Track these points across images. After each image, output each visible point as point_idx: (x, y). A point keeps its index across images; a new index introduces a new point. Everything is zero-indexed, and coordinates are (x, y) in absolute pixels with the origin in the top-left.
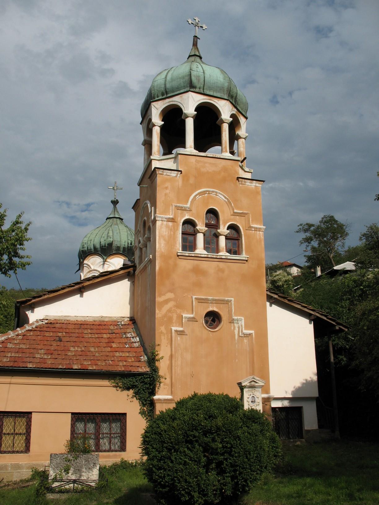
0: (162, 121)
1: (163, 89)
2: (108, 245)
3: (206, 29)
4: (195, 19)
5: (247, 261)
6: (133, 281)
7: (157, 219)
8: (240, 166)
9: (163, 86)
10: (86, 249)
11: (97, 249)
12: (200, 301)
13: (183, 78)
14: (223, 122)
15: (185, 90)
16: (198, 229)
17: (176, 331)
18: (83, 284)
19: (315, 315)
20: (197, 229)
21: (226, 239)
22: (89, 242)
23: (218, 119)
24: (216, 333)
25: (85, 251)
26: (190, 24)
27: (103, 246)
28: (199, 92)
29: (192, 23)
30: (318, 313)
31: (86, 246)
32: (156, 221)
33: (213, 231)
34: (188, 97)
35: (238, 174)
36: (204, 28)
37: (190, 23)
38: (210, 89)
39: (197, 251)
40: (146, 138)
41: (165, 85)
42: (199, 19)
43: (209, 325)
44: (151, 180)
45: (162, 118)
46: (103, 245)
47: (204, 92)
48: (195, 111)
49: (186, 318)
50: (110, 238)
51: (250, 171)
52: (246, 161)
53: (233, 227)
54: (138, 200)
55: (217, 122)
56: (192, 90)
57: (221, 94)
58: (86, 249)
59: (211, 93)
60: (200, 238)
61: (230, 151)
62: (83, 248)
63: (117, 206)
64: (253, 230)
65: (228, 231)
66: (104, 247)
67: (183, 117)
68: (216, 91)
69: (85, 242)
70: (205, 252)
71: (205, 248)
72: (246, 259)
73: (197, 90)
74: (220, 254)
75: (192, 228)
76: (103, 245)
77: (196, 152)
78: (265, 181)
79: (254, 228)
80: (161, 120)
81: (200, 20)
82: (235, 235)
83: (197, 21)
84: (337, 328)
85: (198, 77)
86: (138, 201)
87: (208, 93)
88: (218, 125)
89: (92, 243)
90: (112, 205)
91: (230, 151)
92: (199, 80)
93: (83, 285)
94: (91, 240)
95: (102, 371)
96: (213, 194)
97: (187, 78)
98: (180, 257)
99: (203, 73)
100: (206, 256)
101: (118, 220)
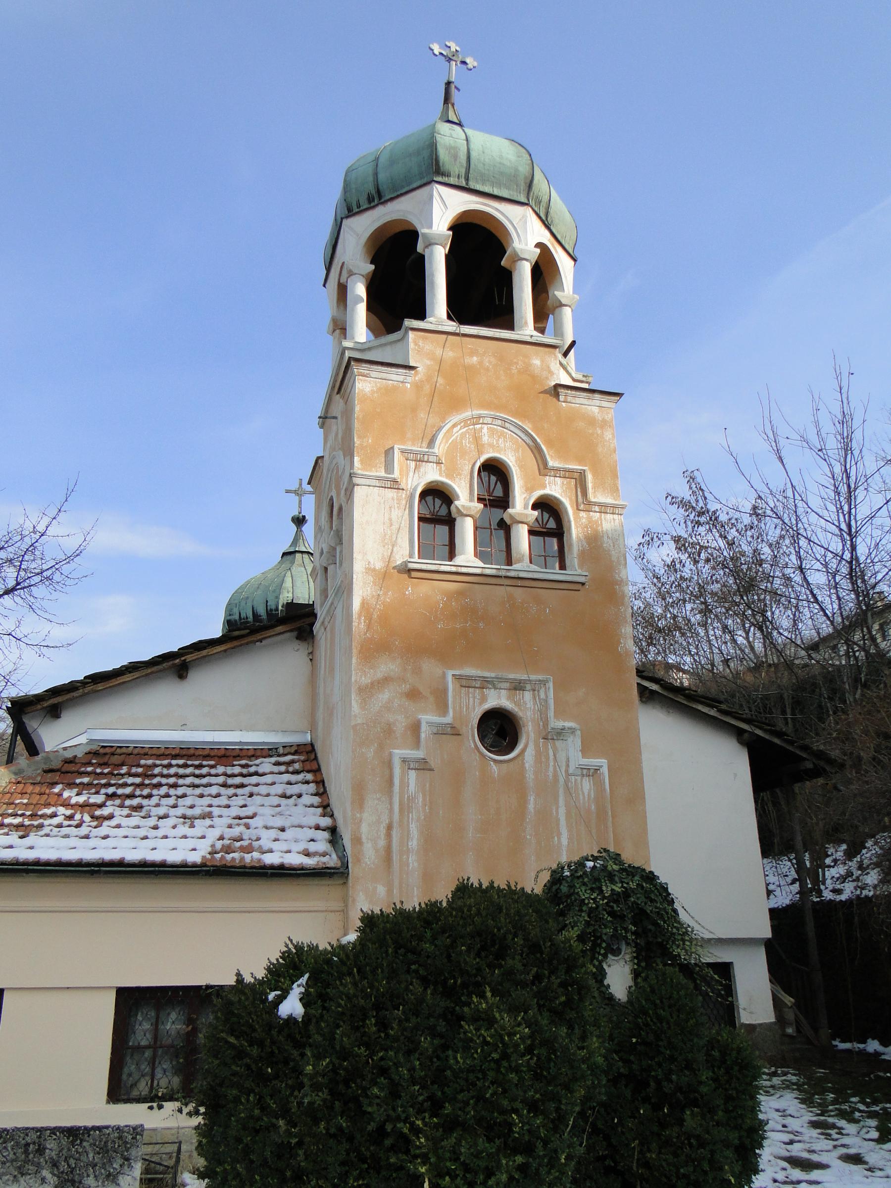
0: (371, 263)
1: (371, 189)
2: (282, 607)
3: (474, 67)
4: (448, 44)
5: (583, 584)
6: (310, 651)
7: (356, 480)
8: (561, 364)
9: (371, 179)
10: (237, 617)
11: (260, 616)
12: (465, 682)
13: (418, 153)
14: (517, 258)
15: (425, 180)
16: (460, 507)
17: (404, 761)
18: (183, 658)
19: (752, 734)
20: (457, 507)
21: (531, 532)
22: (243, 603)
23: (504, 252)
24: (511, 764)
25: (236, 621)
26: (436, 56)
27: (271, 610)
28: (457, 184)
29: (441, 54)
30: (761, 728)
31: (236, 611)
32: (354, 485)
33: (497, 514)
34: (431, 198)
35: (558, 379)
36: (470, 66)
37: (436, 52)
38: (484, 180)
39: (458, 560)
40: (335, 314)
41: (376, 174)
42: (456, 45)
43: (492, 746)
44: (343, 397)
45: (373, 253)
46: (273, 607)
47: (467, 184)
48: (449, 229)
49: (430, 724)
50: (288, 592)
51: (584, 379)
52: (575, 352)
53: (546, 505)
54: (318, 458)
55: (503, 263)
56: (439, 179)
57: (511, 192)
58: (237, 617)
59: (487, 189)
60: (466, 530)
61: (536, 326)
62: (230, 615)
63: (304, 528)
64: (598, 510)
65: (536, 513)
66: (274, 612)
67: (420, 248)
68: (500, 185)
69: (236, 602)
70: (480, 564)
71: (477, 554)
72: (582, 579)
73: (452, 181)
74: (515, 567)
75: (444, 507)
76: (273, 607)
77: (452, 326)
78: (622, 394)
79: (600, 505)
80: (369, 261)
81: (459, 47)
82: (552, 524)
83: (453, 49)
84: (809, 765)
85: (454, 152)
86: (320, 461)
87: (479, 187)
88: (504, 269)
89: (249, 605)
90: (293, 528)
91: (536, 326)
92: (455, 157)
93: (185, 660)
94: (247, 598)
95: (204, 868)
96: (496, 423)
97: (426, 154)
98: (414, 574)
99: (465, 142)
100: (478, 571)
101: (306, 556)
